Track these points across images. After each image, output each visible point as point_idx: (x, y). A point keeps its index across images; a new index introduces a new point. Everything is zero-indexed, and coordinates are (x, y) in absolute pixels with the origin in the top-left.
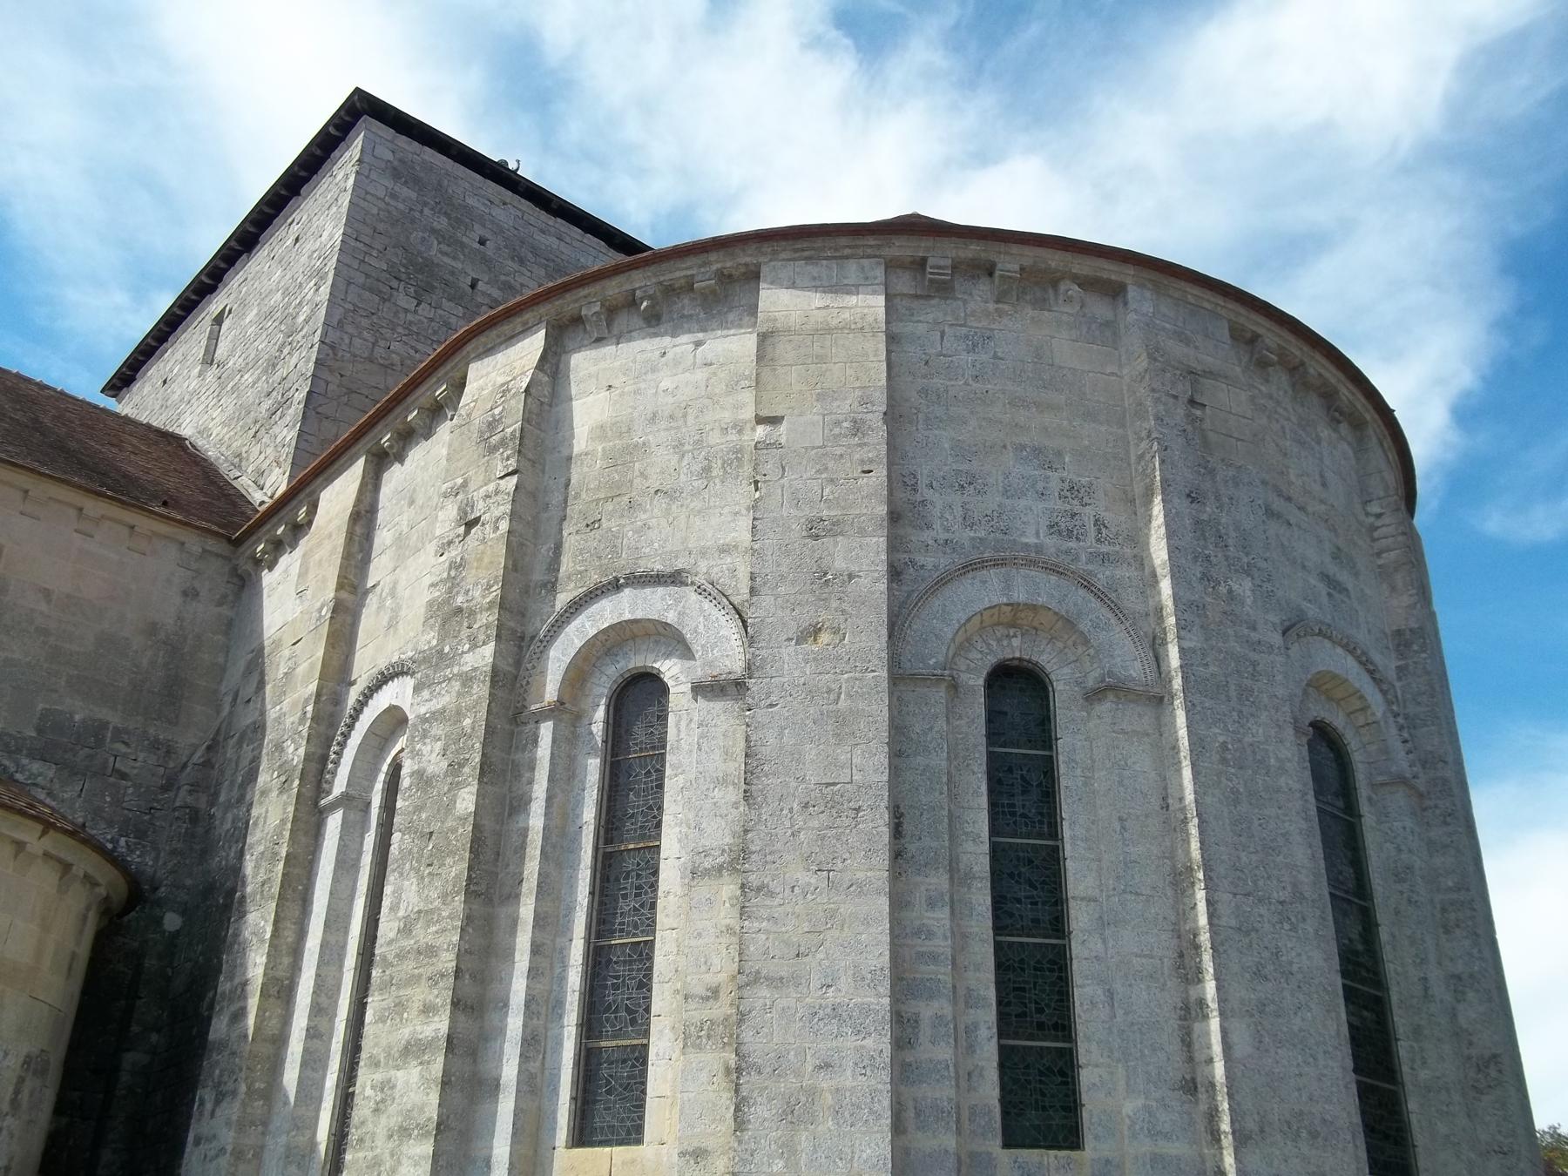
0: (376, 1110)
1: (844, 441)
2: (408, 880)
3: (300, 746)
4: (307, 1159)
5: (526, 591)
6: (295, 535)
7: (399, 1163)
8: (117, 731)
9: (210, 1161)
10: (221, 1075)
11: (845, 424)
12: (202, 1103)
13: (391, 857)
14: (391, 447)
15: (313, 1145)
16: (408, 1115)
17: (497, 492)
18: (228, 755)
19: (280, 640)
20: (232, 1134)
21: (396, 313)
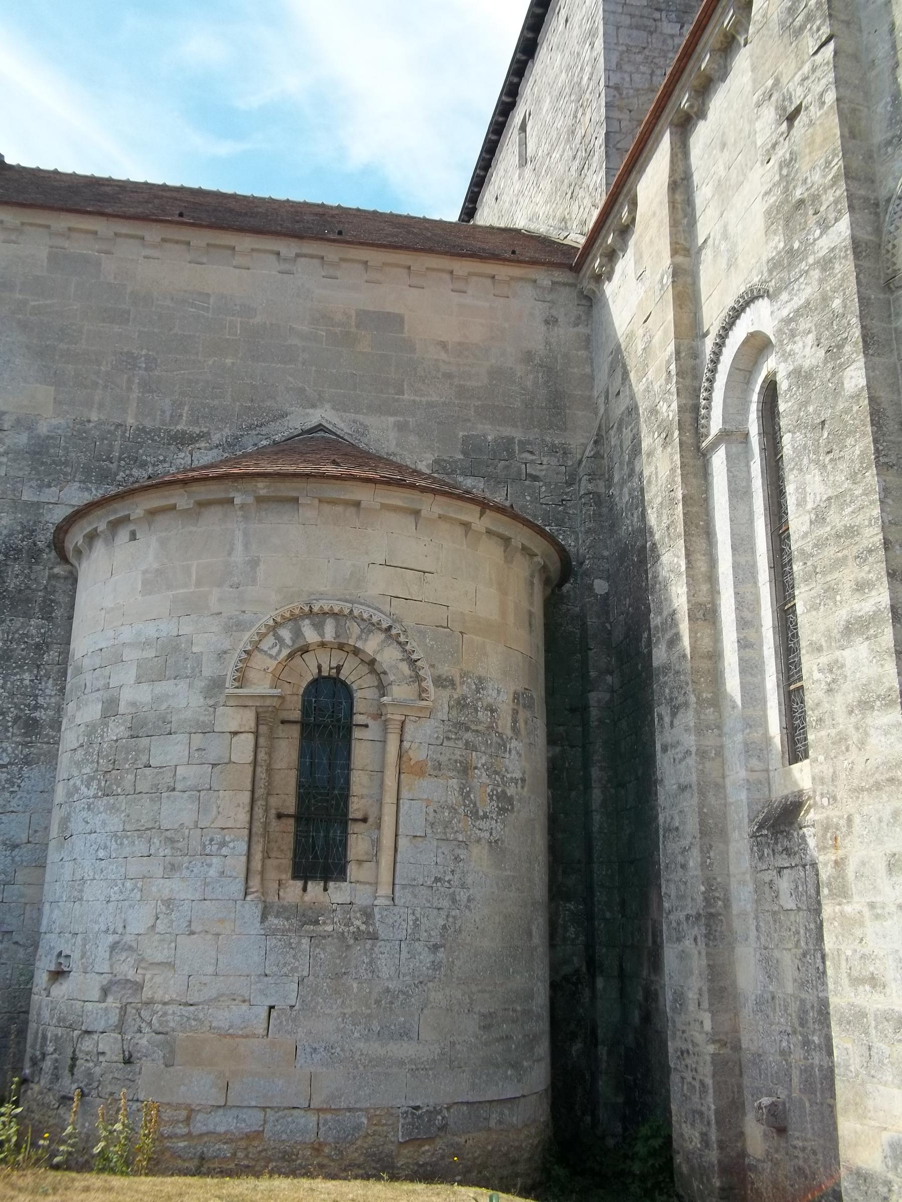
0: (830, 691)
2: (810, 473)
3: (672, 401)
4: (765, 752)
5: (869, 157)
6: (623, 239)
7: (866, 734)
9: (680, 762)
10: (671, 692)
12: (661, 718)
14: (691, 106)
15: (768, 740)
16: (865, 689)
17: (814, 69)
18: (612, 444)
19: (632, 331)
20: (693, 737)
21: (664, 41)
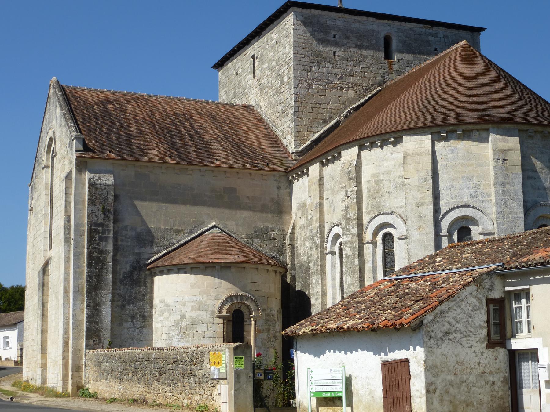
1: (423, 183)
8: (271, 228)
11: (423, 179)
13: (344, 272)
